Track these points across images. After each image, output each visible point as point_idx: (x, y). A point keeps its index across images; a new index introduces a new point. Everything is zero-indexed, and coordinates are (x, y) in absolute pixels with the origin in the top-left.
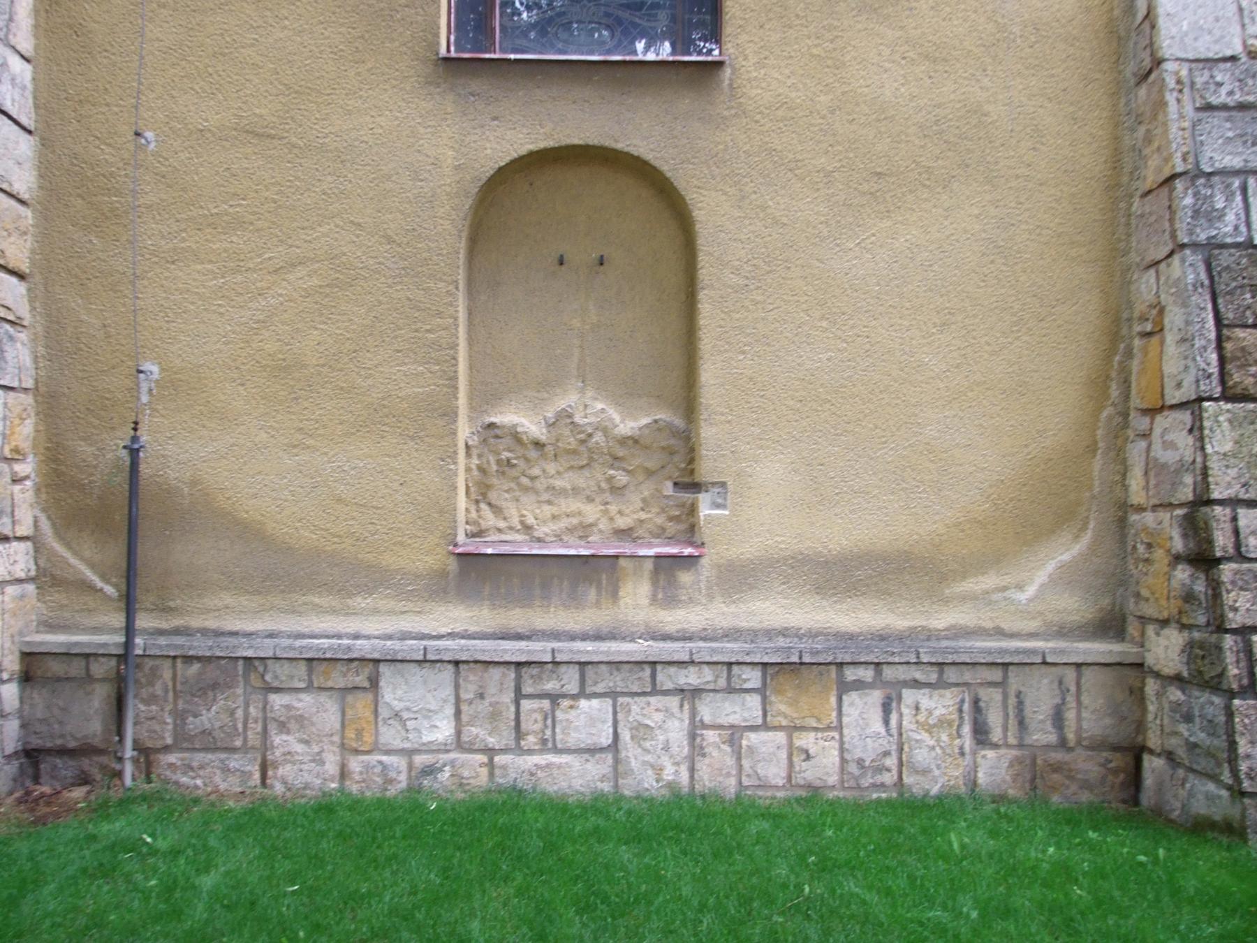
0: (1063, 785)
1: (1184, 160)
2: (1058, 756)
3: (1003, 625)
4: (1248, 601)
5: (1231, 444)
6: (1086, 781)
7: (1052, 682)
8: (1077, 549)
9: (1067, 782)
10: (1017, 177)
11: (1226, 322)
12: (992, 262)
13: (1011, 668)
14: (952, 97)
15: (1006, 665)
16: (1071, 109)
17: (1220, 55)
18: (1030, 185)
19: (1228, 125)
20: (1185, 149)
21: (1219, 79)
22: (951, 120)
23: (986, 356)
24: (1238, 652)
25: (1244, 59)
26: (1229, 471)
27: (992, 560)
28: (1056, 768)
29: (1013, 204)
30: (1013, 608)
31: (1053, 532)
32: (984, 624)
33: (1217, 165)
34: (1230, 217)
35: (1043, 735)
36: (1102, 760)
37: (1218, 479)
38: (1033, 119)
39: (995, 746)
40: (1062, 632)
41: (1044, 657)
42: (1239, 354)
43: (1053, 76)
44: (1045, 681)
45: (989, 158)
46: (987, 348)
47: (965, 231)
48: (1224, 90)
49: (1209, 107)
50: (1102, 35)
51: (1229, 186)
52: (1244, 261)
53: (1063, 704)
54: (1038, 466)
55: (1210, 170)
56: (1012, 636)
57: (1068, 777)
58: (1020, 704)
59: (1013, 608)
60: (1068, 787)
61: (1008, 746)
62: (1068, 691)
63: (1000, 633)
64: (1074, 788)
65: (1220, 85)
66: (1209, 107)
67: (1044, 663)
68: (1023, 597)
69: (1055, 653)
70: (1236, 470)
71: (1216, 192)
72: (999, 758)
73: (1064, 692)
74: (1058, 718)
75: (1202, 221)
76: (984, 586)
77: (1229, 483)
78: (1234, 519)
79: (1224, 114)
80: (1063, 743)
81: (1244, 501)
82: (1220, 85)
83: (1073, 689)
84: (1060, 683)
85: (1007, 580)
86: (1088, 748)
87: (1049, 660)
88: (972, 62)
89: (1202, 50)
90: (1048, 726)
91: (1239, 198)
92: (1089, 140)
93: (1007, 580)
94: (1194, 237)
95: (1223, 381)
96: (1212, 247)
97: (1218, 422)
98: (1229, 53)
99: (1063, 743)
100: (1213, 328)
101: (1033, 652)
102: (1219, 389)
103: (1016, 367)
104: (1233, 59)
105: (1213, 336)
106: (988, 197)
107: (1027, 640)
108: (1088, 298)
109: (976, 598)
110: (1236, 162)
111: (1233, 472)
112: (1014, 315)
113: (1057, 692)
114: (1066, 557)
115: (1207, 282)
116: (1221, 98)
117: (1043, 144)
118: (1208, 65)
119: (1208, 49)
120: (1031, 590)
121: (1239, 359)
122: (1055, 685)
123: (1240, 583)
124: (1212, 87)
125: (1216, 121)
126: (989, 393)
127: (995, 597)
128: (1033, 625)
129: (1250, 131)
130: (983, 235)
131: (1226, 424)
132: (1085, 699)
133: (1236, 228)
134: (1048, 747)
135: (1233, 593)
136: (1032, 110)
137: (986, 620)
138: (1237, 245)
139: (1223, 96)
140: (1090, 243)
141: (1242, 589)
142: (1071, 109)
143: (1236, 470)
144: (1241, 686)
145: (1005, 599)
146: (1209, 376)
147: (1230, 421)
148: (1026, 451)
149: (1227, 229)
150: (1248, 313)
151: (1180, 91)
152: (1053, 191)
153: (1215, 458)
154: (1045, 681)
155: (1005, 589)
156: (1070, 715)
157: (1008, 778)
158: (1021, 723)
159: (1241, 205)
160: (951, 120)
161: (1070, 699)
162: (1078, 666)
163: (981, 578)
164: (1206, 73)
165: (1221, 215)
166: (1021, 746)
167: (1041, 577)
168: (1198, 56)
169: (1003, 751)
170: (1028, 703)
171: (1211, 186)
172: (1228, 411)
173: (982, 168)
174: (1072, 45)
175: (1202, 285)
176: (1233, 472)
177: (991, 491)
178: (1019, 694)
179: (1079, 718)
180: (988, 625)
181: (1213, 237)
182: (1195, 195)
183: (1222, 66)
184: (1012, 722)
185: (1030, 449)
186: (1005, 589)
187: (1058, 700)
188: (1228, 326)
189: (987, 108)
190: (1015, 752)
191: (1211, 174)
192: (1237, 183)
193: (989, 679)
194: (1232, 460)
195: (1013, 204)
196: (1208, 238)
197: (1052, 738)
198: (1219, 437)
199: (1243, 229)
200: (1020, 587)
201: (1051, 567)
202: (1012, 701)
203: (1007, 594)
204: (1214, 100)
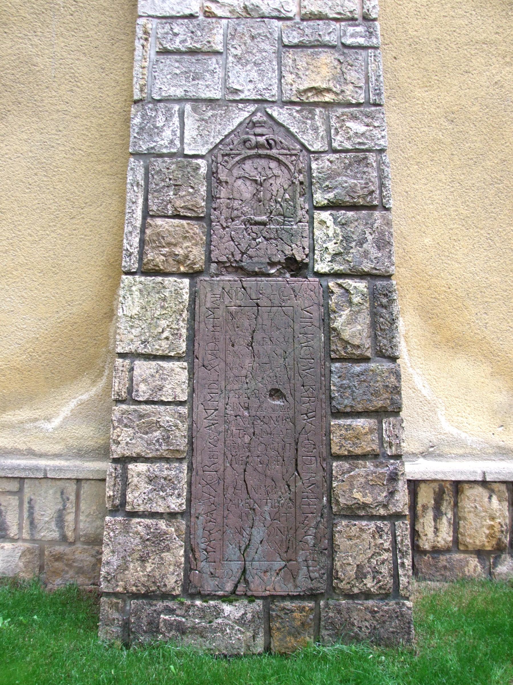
0: (63, 571)
1: (142, 91)
2: (60, 549)
3: (33, 448)
4: (129, 436)
5: (138, 309)
6: (81, 568)
7: (55, 493)
8: (94, 391)
9: (66, 568)
10: (58, 111)
11: (151, 213)
12: (36, 174)
13: (26, 481)
14: (9, 51)
15: (22, 480)
16: (101, 61)
17: (181, 14)
18: (68, 117)
21: (176, 31)
22: (8, 69)
23: (28, 244)
24: (116, 477)
25: (201, 17)
26: (133, 331)
27: (27, 398)
28: (59, 558)
29: (54, 132)
30: (42, 435)
31: (75, 378)
32: (19, 446)
33: (163, 94)
34: (167, 134)
35: (49, 532)
36: (94, 553)
37: (123, 337)
38: (71, 68)
39: (13, 540)
40: (81, 454)
41: (46, 474)
43: (88, 37)
44: (51, 492)
45: (36, 97)
46: (29, 238)
47: (17, 151)
48: (178, 40)
49: (165, 52)
50: (126, 7)
51: (169, 110)
53: (64, 509)
54: (66, 327)
55: (158, 98)
56: (41, 456)
57: (67, 565)
58: (31, 508)
59: (42, 435)
60: (67, 572)
61: (25, 540)
62: (68, 499)
63: (31, 453)
64: (71, 573)
65: (176, 35)
66: (165, 52)
67: (46, 478)
68: (50, 426)
69: (54, 470)
71: (160, 113)
72: (14, 550)
73: (65, 500)
74: (60, 519)
75: (145, 136)
76: (20, 418)
77: (132, 340)
78: (132, 369)
79: (177, 57)
80: (64, 538)
81: (142, 354)
82: (176, 35)
83: (72, 498)
84: (62, 493)
85: (38, 413)
86: (84, 543)
87: (49, 476)
88: (26, 26)
89: (168, 9)
90: (53, 525)
91: (176, 120)
92: (113, 84)
93: (38, 413)
94: (137, 148)
96: (153, 154)
97: (130, 291)
98: (187, 12)
99: (64, 538)
100: (140, 218)
101: (37, 469)
102: (137, 265)
103: (51, 253)
104: (191, 16)
105: (138, 224)
106: (35, 126)
107: (53, 459)
108: (110, 201)
109: (14, 427)
110: (179, 93)
111: (135, 332)
112: (51, 213)
113: (60, 500)
114: (85, 397)
116: (177, 44)
117: (78, 87)
118: (169, 21)
119: (172, 9)
120: (56, 422)
121: (154, 241)
122: (58, 495)
123: (125, 421)
124: (170, 37)
126: (29, 272)
127: (28, 426)
128: (57, 448)
129: (193, 69)
130: (30, 154)
131: (137, 293)
132: (83, 506)
133: (172, 142)
134: (52, 542)
135: (118, 429)
136: (70, 61)
137: (20, 442)
138: (171, 155)
139: (177, 43)
140: (113, 161)
141: (126, 426)
142: (101, 61)
144: (113, 506)
145: (36, 428)
146: (131, 254)
147: (141, 291)
148: (57, 316)
149: (162, 143)
150: (169, 206)
151: (146, 40)
152: (85, 122)
153: (124, 320)
154: (51, 492)
155: (36, 420)
156: (70, 518)
157: (21, 564)
158: (32, 523)
159: (177, 123)
160: (8, 69)
161: (71, 507)
162: (78, 481)
163: (17, 412)
164: (167, 26)
165: (161, 130)
166: (33, 540)
167: (66, 411)
168: (164, 14)
169: (20, 543)
170: (37, 508)
171: (156, 110)
172: (141, 283)
173: (30, 105)
174: (103, 14)
175: (138, 184)
176: (135, 332)
177: (28, 346)
178: (30, 501)
179: (76, 521)
180: (22, 447)
181: (152, 148)
182: (143, 116)
183: (180, 21)
184: (26, 523)
185: (61, 314)
186: (36, 420)
187: (60, 506)
188: (153, 216)
189: (36, 60)
190: (27, 545)
191: (159, 101)
193: (8, 489)
194: (137, 322)
195: (54, 132)
197: (56, 535)
199: (177, 142)
200: (48, 419)
201: (73, 404)
202: (26, 505)
203: (37, 424)
204: (169, 46)
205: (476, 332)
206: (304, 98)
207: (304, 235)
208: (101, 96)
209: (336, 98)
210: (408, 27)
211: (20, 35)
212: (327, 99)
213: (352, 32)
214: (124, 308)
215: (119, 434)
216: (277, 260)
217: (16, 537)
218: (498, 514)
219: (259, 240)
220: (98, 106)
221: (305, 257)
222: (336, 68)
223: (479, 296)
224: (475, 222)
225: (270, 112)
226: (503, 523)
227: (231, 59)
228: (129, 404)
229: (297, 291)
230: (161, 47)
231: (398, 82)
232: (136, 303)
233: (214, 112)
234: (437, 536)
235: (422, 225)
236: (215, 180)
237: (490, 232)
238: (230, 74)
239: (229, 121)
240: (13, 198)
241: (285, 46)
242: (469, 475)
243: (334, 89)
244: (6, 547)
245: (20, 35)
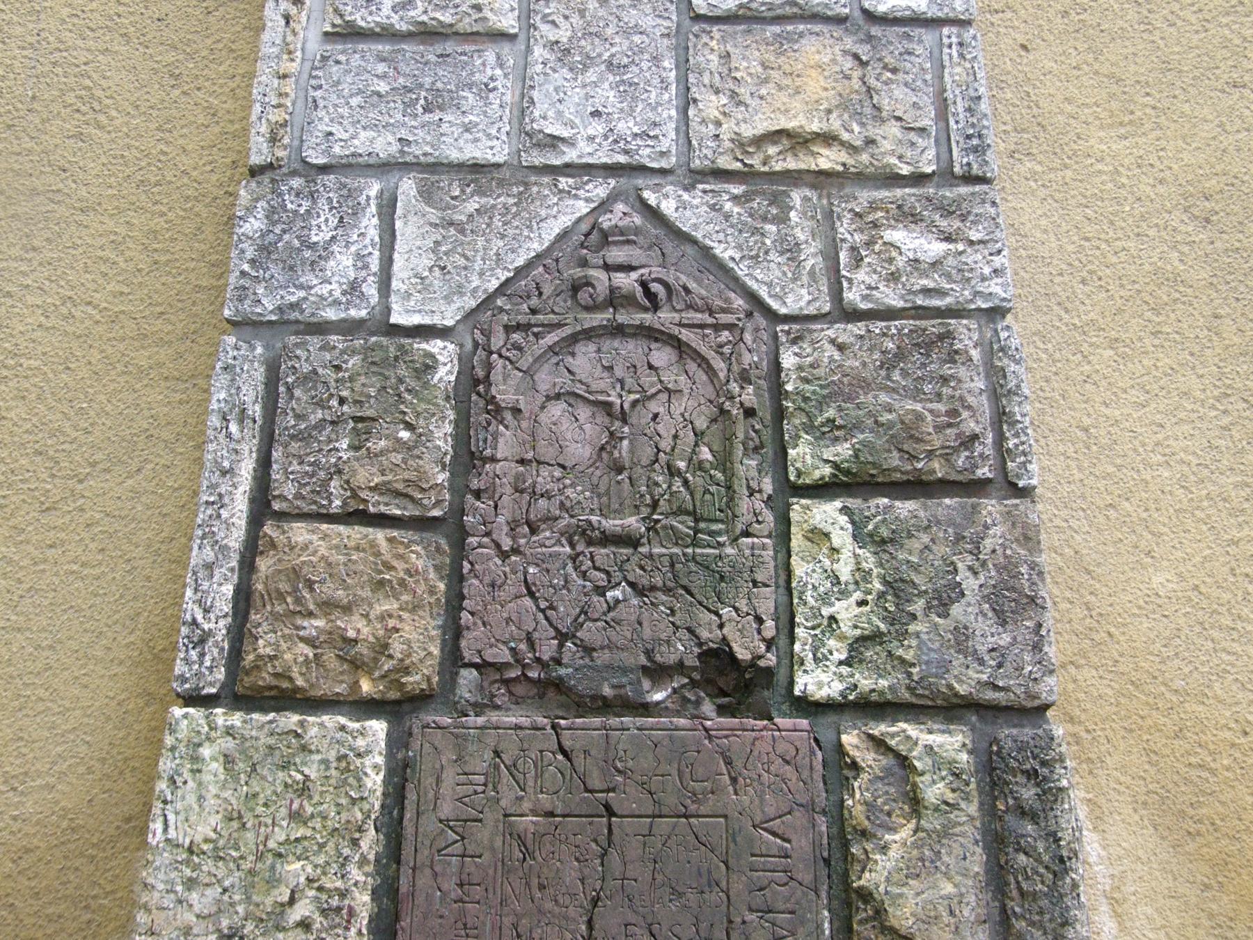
1: (274, 139)
5: (214, 820)
11: (276, 506)
16: (170, 57)
18: (62, 210)
19: (381, 68)
20: (276, 116)
26: (194, 896)
29: (15, 252)
33: (337, 150)
34: (342, 263)
42: (284, 586)
52: (353, 362)
55: (321, 161)
66: (349, 34)
70: (213, 892)
71: (322, 203)
75: (275, 269)
79: (384, 48)
91: (370, 223)
95: (235, 656)
96: (299, 325)
97: (196, 759)
100: (241, 522)
102: (220, 674)
105: (236, 538)
110: (384, 145)
115: (256, 410)
117: (100, 127)
121: (281, 597)
125: (356, 60)
133: (354, 288)
138: (349, 328)
143: (213, 892)
147: (228, 760)
149: (324, 290)
152: (111, 224)
159: (373, 234)
165: (324, 252)
171: (312, 196)
172: (229, 732)
175: (242, 416)
176: (202, 900)
181: (293, 306)
182: (270, 214)
191: (324, 169)
192: (374, 188)
194: (208, 866)
196: (280, 309)
198: (191, 799)
199: (371, 290)
206: (755, 161)
212: (824, 164)
219: (617, 593)
220: (153, 179)
222: (848, 78)
230: (338, 21)
233: (484, 200)
235: (1139, 529)
238: (535, 94)
241: (698, 18)
243: (845, 136)
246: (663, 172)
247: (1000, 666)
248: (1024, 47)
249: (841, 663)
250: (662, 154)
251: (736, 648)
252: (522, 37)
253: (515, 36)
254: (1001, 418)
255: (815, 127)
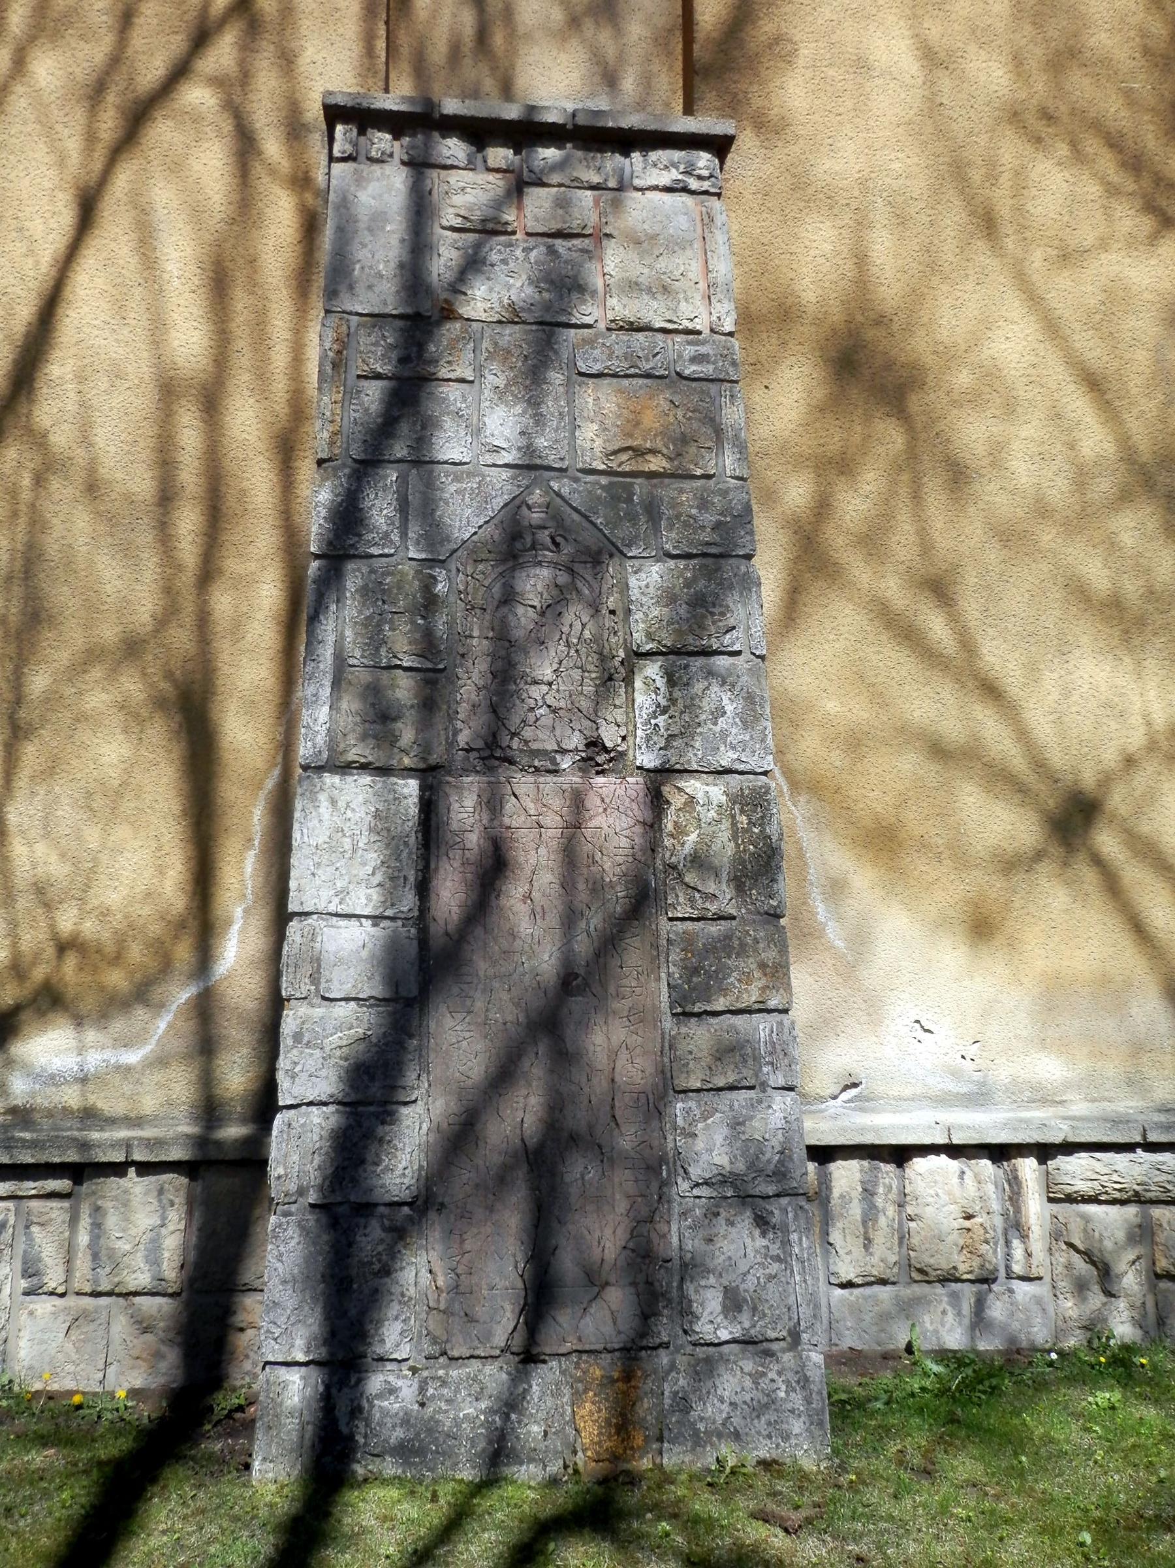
205: (923, 869)
206: (614, 465)
207: (617, 702)
208: (245, 439)
209: (668, 466)
210: (787, 338)
211: (95, 322)
212: (653, 468)
213: (692, 353)
214: (305, 831)
215: (296, 1060)
216: (571, 747)
217: (61, 1290)
218: (977, 1208)
219: (541, 711)
220: (241, 457)
221: (620, 740)
222: (667, 415)
223: (925, 805)
224: (912, 672)
225: (556, 488)
226: (987, 1225)
227: (487, 393)
228: (312, 1005)
229: (607, 800)
230: (366, 368)
231: (772, 428)
232: (326, 824)
233: (459, 485)
234: (871, 1254)
235: (821, 677)
236: (463, 605)
237: (940, 690)
238: (486, 419)
239: (486, 502)
240: (75, 621)
241: (581, 374)
242: (921, 1134)
243: (665, 451)
244: (39, 1312)
245: (95, 322)
246: (560, 470)
247: (744, 750)
248: (766, 387)
249: (661, 749)
250: (561, 459)
251: (606, 741)
252: (476, 382)
253: (472, 382)
254: (698, 1015)
255: (648, 445)
